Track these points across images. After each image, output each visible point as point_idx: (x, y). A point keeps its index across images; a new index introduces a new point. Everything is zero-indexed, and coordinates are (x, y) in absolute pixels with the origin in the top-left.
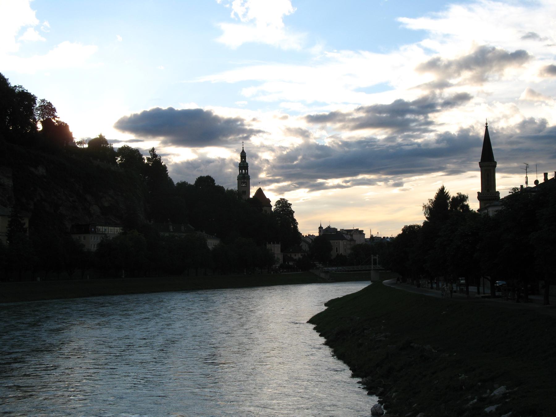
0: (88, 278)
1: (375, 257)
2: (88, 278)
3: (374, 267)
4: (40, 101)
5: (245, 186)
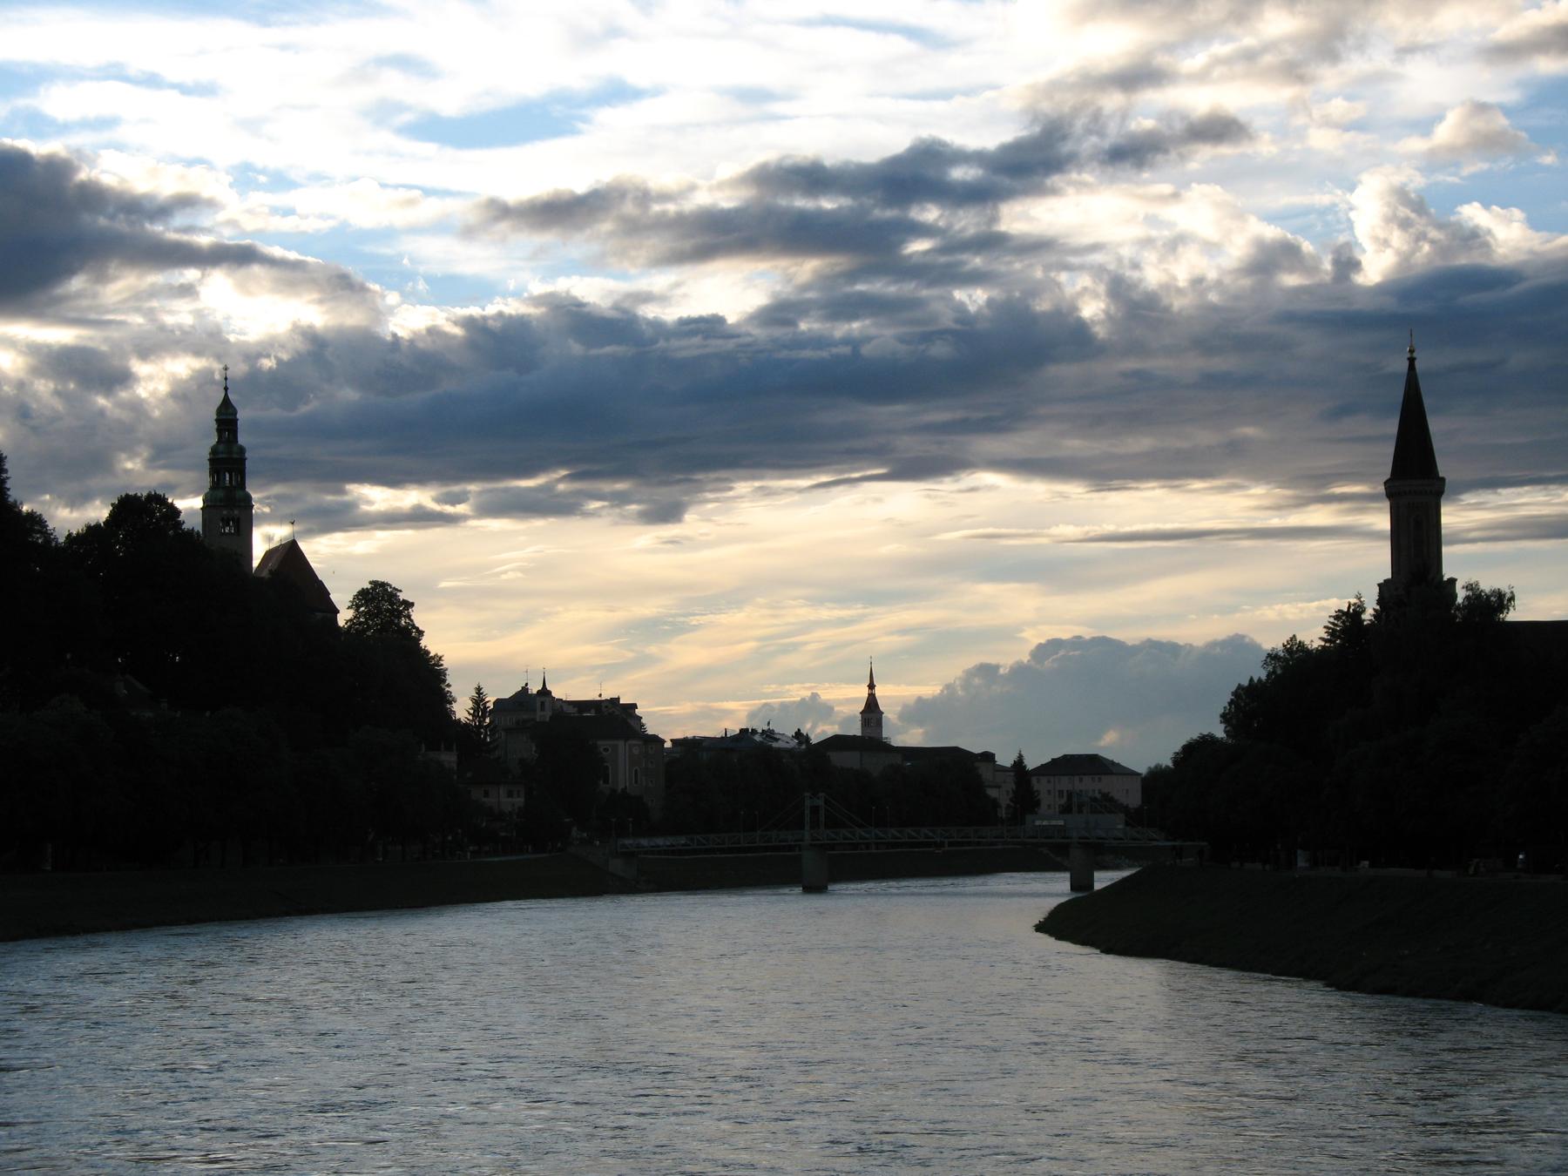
0: (469, 857)
2: (469, 857)
5: (230, 533)
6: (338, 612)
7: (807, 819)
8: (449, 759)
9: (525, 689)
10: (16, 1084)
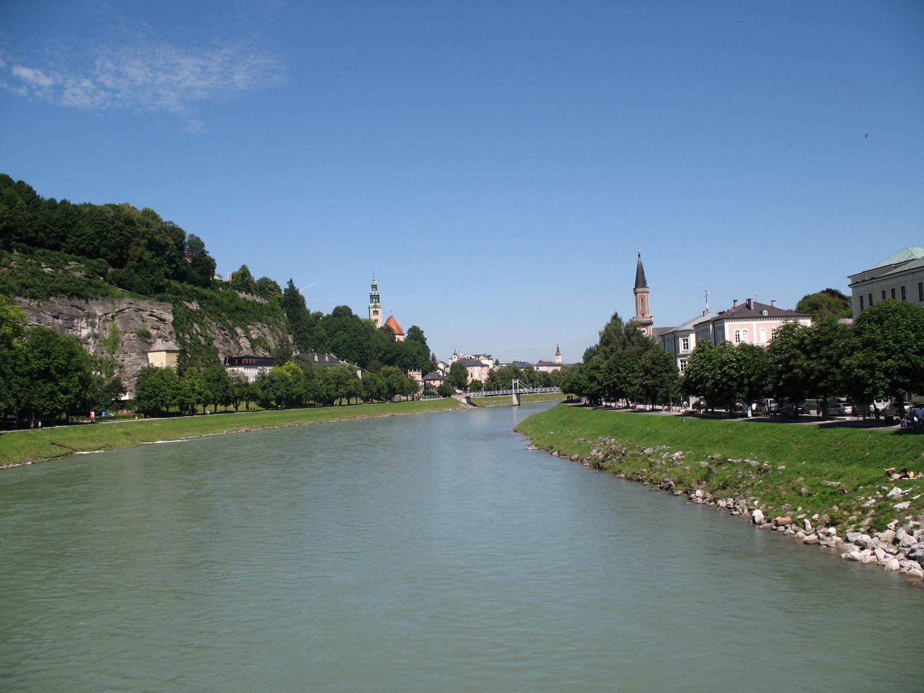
1: (516, 382)
4: (188, 236)
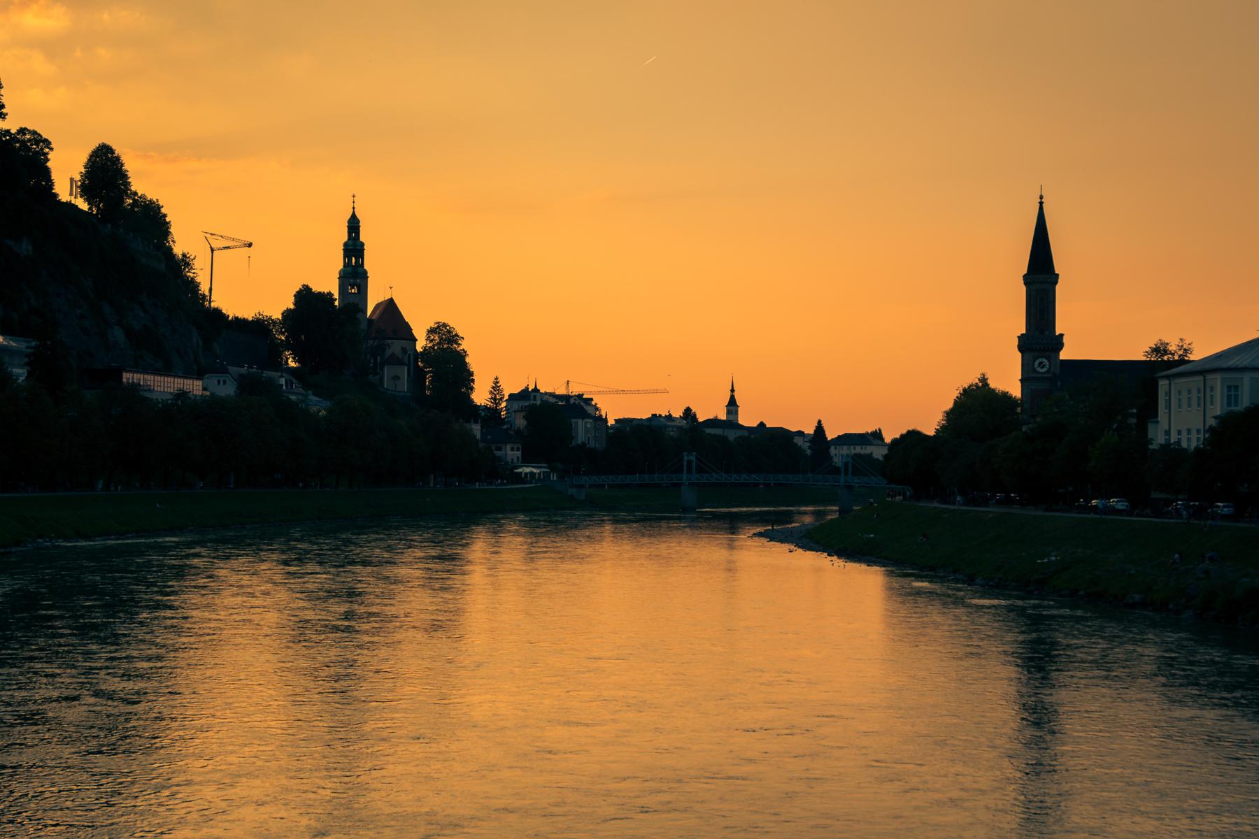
3: (725, 478)
5: (355, 293)
6: (417, 340)
7: (685, 468)
8: (476, 429)
9: (527, 388)
10: (118, 661)
